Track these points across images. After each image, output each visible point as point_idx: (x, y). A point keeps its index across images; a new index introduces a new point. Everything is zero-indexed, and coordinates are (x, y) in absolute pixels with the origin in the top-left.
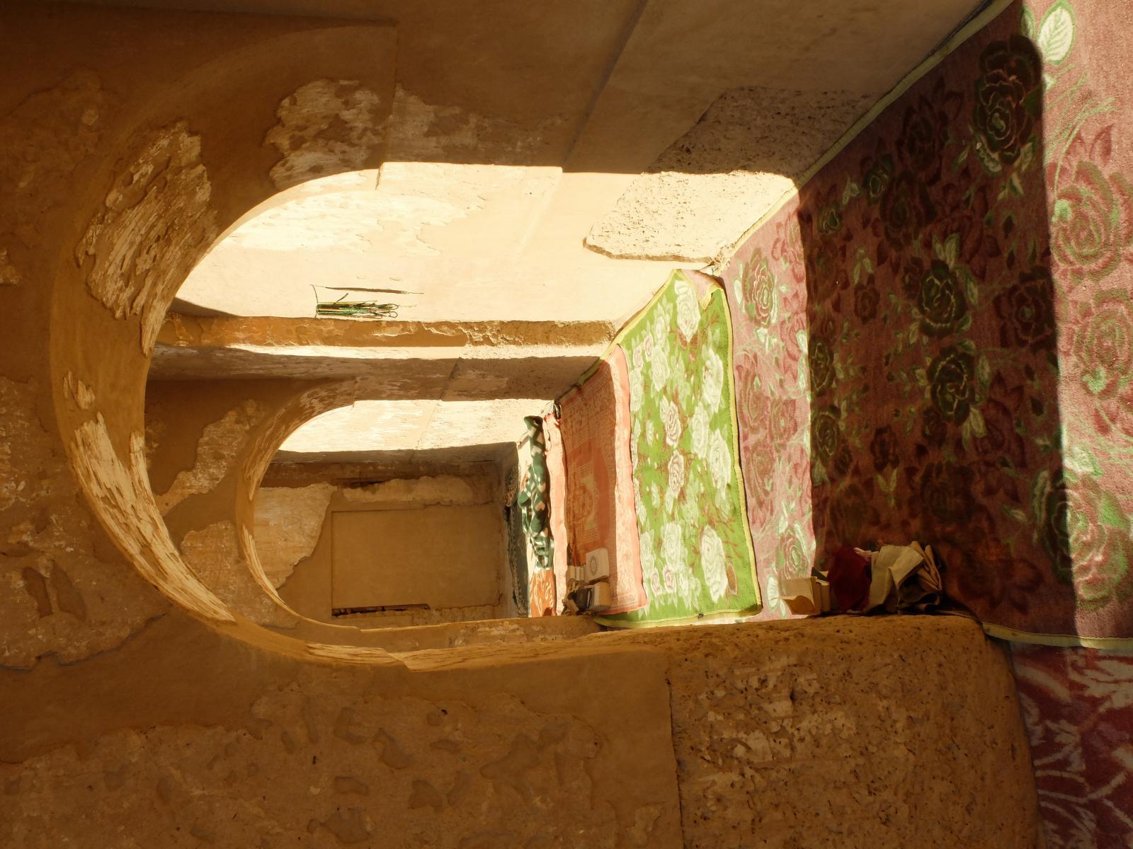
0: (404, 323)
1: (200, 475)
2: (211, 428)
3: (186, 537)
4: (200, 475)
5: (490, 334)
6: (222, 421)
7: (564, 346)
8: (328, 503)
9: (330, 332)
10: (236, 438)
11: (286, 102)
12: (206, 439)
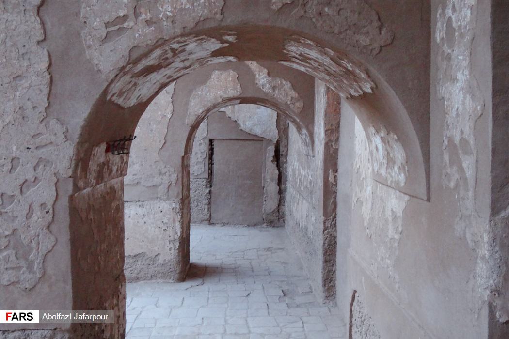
0: (336, 185)
1: (265, 79)
2: (290, 85)
3: (235, 72)
4: (265, 79)
5: (330, 230)
6: (293, 91)
7: (322, 271)
8: (267, 138)
9: (332, 146)
10: (284, 97)
11: (395, 137)
12: (284, 82)
